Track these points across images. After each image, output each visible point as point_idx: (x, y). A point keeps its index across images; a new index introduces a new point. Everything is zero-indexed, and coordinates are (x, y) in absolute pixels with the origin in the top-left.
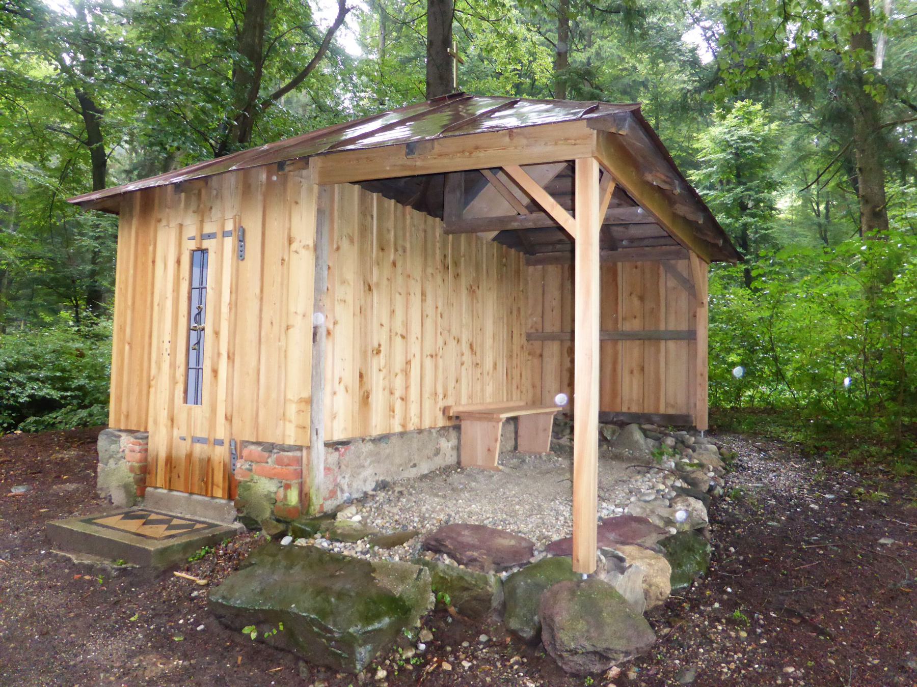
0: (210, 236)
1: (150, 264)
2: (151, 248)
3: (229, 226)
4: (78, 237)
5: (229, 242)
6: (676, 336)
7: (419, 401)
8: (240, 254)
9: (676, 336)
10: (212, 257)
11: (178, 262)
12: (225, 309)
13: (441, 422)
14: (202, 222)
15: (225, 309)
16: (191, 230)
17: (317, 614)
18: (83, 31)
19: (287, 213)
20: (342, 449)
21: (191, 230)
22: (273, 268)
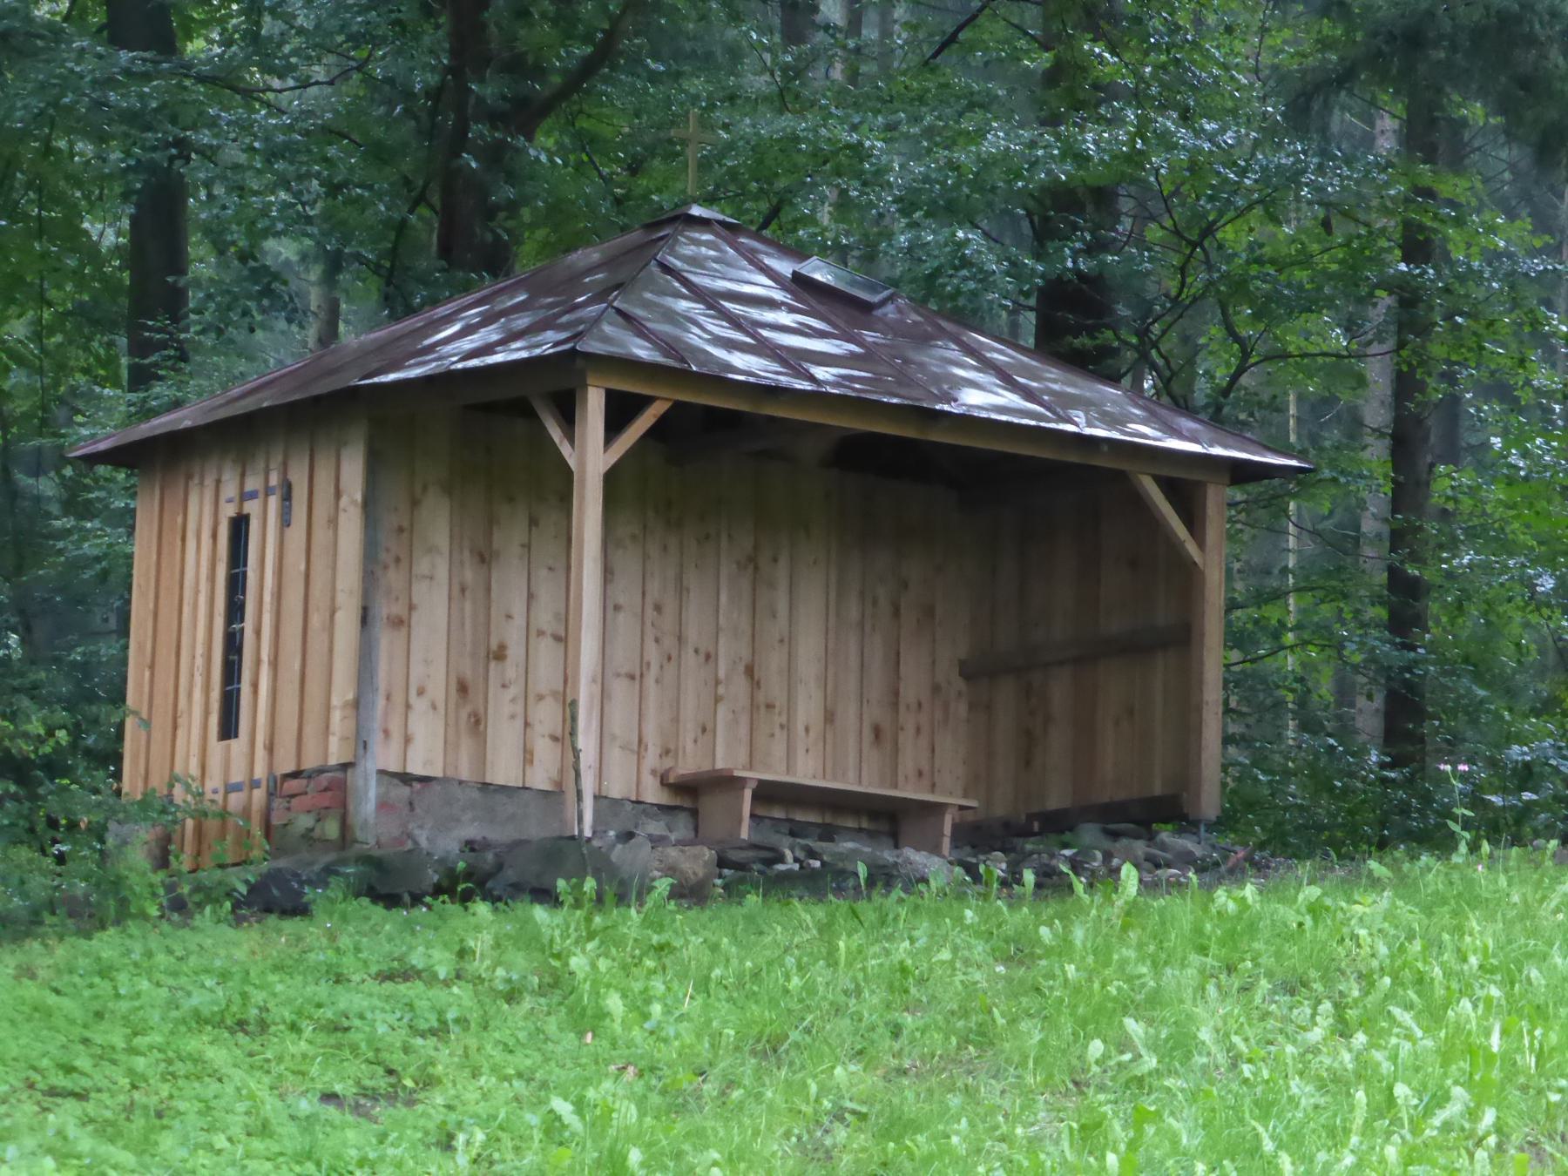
0: (253, 495)
1: (179, 543)
2: (180, 519)
3: (274, 480)
4: (68, 522)
5: (274, 502)
6: (425, 577)
7: (310, 633)
8: (285, 521)
9: (425, 577)
10: (254, 526)
11: (214, 536)
12: (267, 598)
13: (653, 794)
14: (243, 475)
15: (267, 598)
16: (230, 490)
17: (100, 397)
18: (305, 899)
19: (333, 460)
20: (417, 786)
21: (230, 490)
22: (321, 535)
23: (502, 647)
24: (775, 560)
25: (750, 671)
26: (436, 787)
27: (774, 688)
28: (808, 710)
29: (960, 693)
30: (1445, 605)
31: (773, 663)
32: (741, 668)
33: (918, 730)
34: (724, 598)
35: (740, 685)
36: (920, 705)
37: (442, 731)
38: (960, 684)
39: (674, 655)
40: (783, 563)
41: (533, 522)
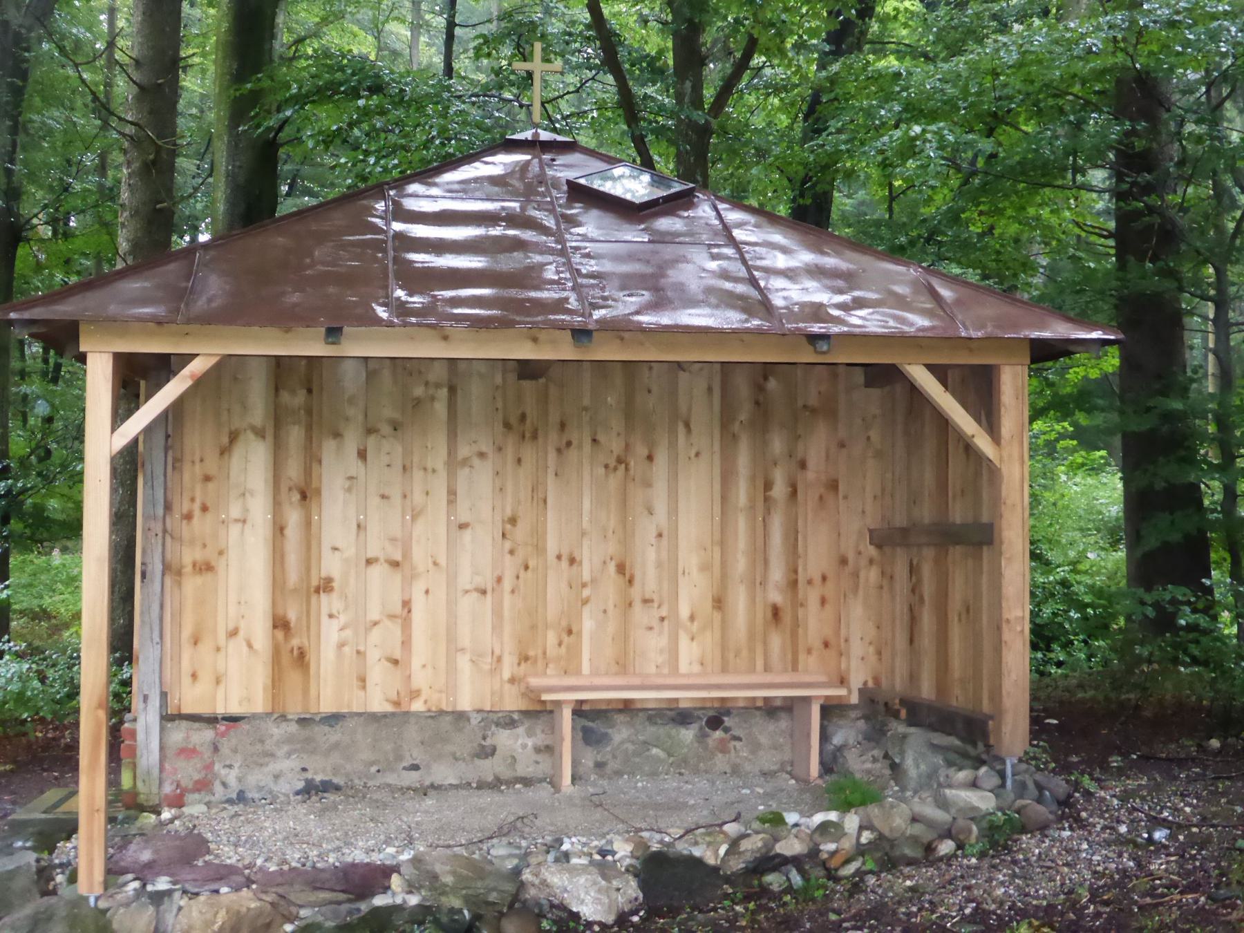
6: (237, 521)
23: (329, 580)
24: (650, 458)
25: (621, 569)
26: (244, 726)
27: (649, 579)
28: (692, 592)
29: (871, 562)
30: (943, 129)
31: (648, 560)
32: (612, 567)
33: (823, 601)
34: (587, 504)
35: (611, 583)
36: (824, 578)
37: (322, 671)
38: (872, 551)
39: (442, 561)
40: (661, 458)
41: (454, 463)
